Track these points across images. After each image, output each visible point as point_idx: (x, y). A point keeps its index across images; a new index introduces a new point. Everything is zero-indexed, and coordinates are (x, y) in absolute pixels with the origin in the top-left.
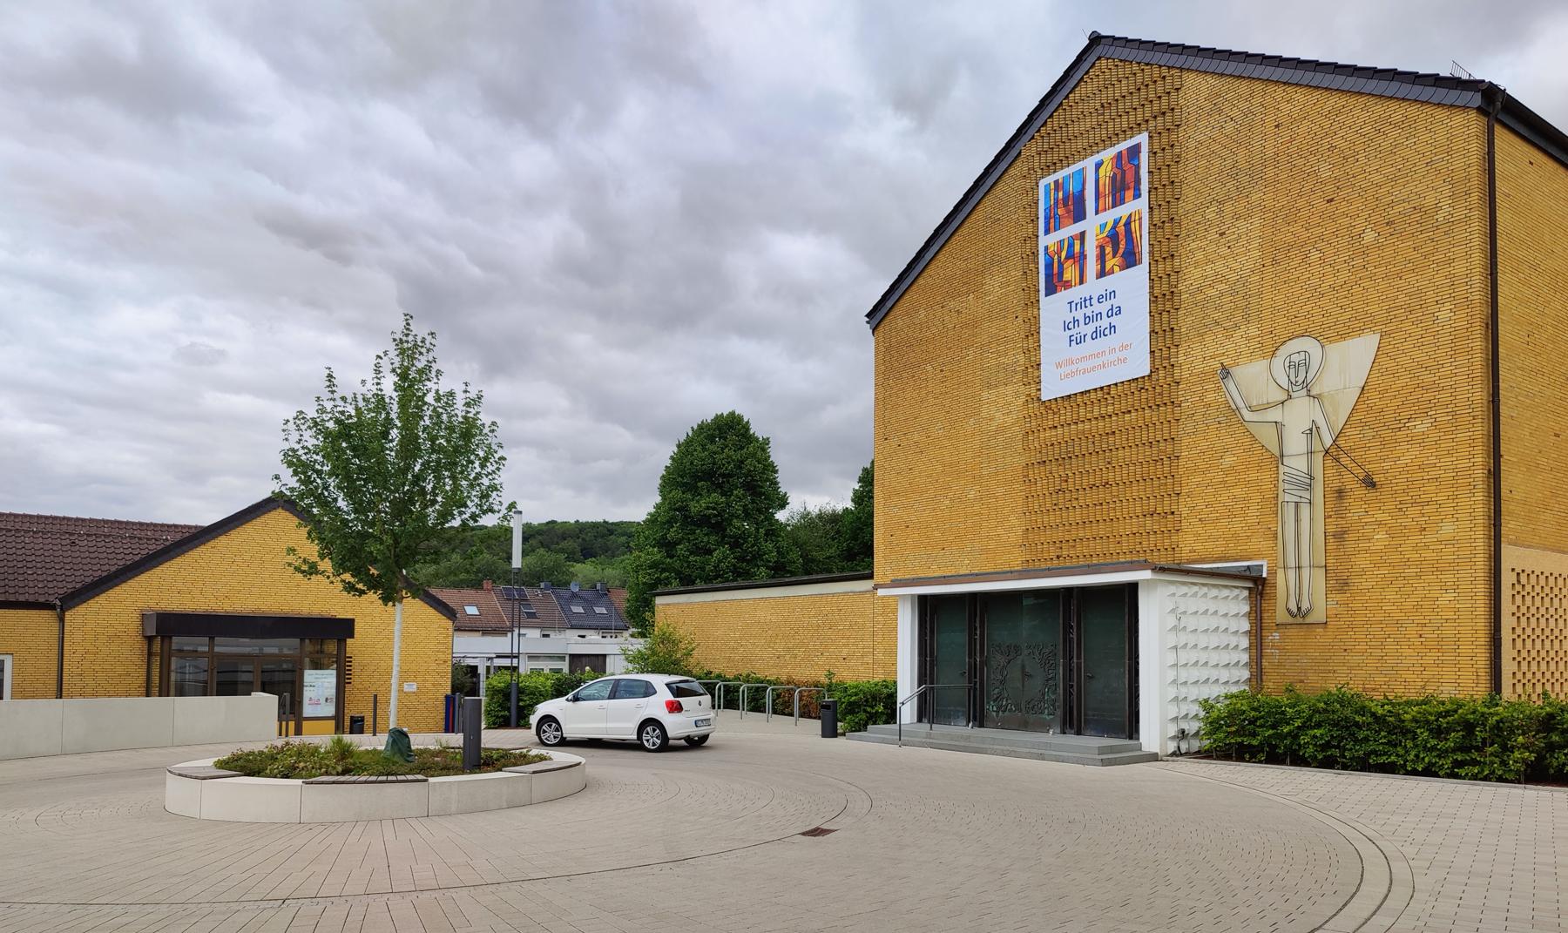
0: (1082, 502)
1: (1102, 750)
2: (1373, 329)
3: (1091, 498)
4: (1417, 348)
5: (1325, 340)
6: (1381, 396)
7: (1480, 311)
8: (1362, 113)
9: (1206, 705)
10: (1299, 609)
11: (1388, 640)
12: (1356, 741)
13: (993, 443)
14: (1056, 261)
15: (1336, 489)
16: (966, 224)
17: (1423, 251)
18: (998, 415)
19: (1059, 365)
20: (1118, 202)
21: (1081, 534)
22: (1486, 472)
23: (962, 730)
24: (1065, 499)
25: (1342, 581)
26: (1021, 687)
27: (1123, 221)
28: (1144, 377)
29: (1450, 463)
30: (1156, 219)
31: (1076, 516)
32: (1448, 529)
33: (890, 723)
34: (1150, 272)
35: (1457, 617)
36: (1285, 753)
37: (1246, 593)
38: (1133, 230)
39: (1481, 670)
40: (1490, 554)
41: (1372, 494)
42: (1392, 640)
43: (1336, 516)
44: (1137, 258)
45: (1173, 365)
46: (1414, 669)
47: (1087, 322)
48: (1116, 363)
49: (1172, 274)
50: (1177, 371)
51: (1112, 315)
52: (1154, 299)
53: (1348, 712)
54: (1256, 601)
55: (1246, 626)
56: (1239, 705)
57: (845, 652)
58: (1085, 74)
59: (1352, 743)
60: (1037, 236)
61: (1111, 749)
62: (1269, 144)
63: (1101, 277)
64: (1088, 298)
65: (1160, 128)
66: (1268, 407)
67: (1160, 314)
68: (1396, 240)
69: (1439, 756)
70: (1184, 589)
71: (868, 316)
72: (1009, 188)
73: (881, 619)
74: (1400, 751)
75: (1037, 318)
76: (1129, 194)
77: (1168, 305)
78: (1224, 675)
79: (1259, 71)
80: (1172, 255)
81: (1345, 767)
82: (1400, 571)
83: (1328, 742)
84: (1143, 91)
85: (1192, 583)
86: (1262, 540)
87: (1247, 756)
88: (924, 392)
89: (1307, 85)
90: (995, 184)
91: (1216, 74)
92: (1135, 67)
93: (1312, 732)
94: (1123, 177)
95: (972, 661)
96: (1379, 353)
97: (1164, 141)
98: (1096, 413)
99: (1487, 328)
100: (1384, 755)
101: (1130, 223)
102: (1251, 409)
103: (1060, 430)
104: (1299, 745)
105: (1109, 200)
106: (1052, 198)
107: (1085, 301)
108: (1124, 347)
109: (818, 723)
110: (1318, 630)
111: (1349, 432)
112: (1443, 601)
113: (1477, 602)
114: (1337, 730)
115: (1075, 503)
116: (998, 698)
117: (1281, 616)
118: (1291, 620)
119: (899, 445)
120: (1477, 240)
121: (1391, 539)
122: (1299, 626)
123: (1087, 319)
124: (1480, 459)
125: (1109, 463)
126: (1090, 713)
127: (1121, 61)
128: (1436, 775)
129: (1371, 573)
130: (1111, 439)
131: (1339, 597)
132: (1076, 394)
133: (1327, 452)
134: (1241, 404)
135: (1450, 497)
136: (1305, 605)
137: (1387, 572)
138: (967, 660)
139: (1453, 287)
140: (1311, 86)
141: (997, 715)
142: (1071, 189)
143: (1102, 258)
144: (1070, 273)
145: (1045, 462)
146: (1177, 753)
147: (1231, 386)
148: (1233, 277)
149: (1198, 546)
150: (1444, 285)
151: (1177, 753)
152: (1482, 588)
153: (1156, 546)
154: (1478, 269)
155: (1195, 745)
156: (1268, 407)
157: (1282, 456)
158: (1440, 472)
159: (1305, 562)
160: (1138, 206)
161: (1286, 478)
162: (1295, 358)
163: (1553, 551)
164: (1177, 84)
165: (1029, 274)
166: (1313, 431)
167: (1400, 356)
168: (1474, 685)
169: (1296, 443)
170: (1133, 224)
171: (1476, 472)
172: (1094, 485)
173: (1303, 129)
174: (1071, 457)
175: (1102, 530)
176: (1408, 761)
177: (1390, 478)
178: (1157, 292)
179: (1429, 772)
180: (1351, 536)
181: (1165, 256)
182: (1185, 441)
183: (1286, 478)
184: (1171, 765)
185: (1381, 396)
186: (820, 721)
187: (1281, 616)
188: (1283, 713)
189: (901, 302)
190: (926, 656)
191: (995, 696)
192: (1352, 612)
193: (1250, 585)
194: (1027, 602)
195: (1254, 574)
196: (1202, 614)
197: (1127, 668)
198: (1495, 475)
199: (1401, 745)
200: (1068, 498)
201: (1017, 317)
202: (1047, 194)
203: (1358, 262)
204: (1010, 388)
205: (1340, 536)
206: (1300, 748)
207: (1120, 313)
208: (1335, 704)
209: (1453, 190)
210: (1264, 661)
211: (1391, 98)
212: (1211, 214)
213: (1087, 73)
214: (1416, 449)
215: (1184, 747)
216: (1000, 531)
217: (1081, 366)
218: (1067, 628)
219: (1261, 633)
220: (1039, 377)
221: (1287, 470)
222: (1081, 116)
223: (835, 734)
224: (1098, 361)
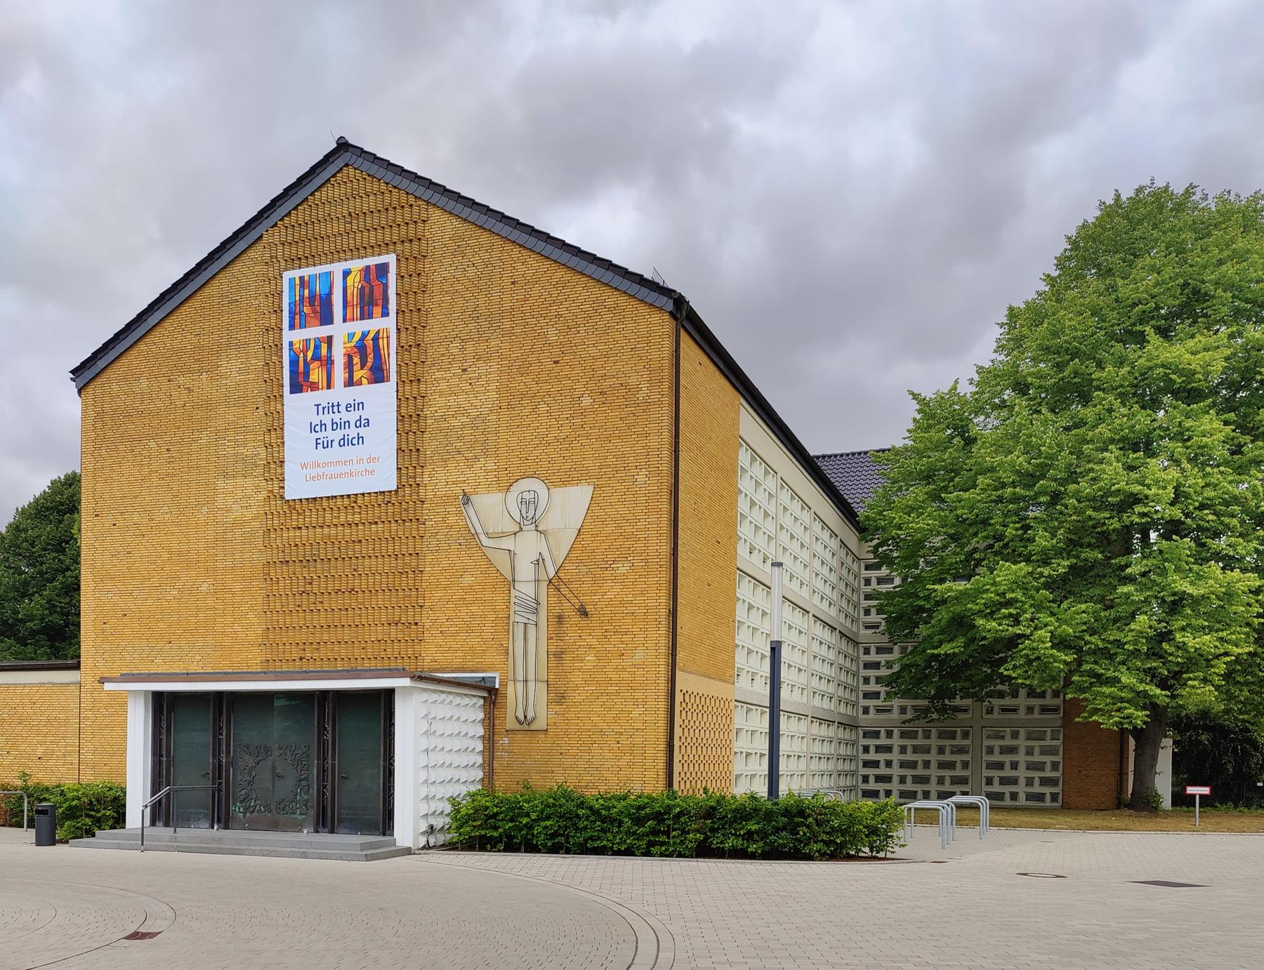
0: (326, 606)
1: (364, 847)
2: (588, 481)
3: (336, 602)
4: (621, 503)
5: (550, 484)
6: (593, 539)
7: (667, 481)
8: (583, 292)
9: (453, 800)
10: (525, 717)
11: (594, 745)
12: (577, 829)
13: (229, 535)
14: (301, 359)
15: (557, 614)
16: (199, 297)
17: (627, 422)
18: (235, 507)
19: (304, 466)
20: (366, 315)
21: (325, 637)
22: (667, 611)
23: (203, 832)
24: (308, 601)
25: (560, 695)
26: (272, 788)
27: (371, 336)
28: (390, 492)
29: (643, 602)
30: (403, 342)
31: (322, 619)
32: (639, 656)
33: (116, 828)
34: (397, 391)
35: (644, 727)
36: (520, 843)
37: (481, 702)
38: (381, 346)
39: (661, 770)
40: (668, 678)
41: (584, 622)
42: (597, 745)
43: (556, 638)
44: (385, 375)
45: (418, 484)
46: (612, 769)
47: (335, 428)
48: (364, 473)
49: (418, 397)
50: (422, 491)
51: (360, 426)
52: (401, 418)
53: (571, 805)
54: (490, 709)
55: (481, 732)
56: (484, 802)
57: (40, 751)
58: (332, 177)
59: (574, 831)
60: (281, 330)
61: (371, 846)
62: (506, 297)
63: (349, 386)
64: (335, 404)
65: (407, 254)
66: (502, 535)
67: (407, 433)
68: (607, 408)
69: (638, 839)
70: (435, 697)
71: (73, 372)
72: (249, 268)
73: (89, 714)
74: (610, 836)
75: (280, 414)
76: (377, 310)
77: (414, 428)
78: (464, 775)
79: (498, 227)
80: (419, 380)
81: (568, 852)
82: (605, 688)
83: (556, 831)
84: (391, 212)
85: (441, 692)
87: (489, 846)
88: (146, 471)
89: (539, 253)
90: (232, 261)
91: (460, 217)
92: (383, 186)
93: (543, 824)
94: (371, 292)
95: (216, 761)
96: (592, 502)
97: (411, 267)
98: (342, 519)
99: (671, 494)
100: (598, 840)
101: (378, 339)
102: (487, 534)
103: (304, 532)
104: (533, 835)
105: (357, 311)
106: (297, 293)
107: (333, 406)
108: (371, 460)
109: (32, 832)
110: (540, 736)
111: (567, 566)
112: (635, 714)
113: (659, 716)
114: (563, 821)
115: (319, 606)
116: (245, 799)
117: (511, 723)
118: (518, 727)
119: (114, 525)
120: (667, 422)
122: (524, 732)
123: (335, 425)
124: (664, 600)
125: (355, 570)
126: (343, 812)
127: (369, 175)
128: (633, 854)
130: (357, 547)
131: (557, 708)
132: (322, 498)
133: (550, 582)
134: (480, 531)
135: (642, 630)
136: (530, 715)
137: (594, 688)
138: (211, 760)
139: (648, 457)
140: (542, 255)
141: (245, 817)
142: (318, 289)
143: (349, 366)
144: (316, 375)
145: (288, 561)
146: (427, 847)
147: (471, 511)
148: (474, 413)
149: (438, 657)
150: (642, 454)
151: (427, 847)
152: (663, 705)
153: (400, 654)
154: (667, 446)
155: (441, 839)
156: (502, 535)
157: (514, 581)
158: (635, 608)
159: (531, 676)
160: (386, 324)
161: (517, 601)
162: (527, 496)
163: (704, 676)
164: (424, 215)
165: (271, 365)
166: (539, 563)
167: (608, 507)
168: (655, 782)
169: (525, 571)
170: (381, 341)
171: (661, 610)
172: (340, 590)
173: (535, 291)
174: (316, 560)
175: (347, 635)
176: (614, 844)
177: (598, 609)
178: (403, 411)
179: (629, 852)
180: (567, 657)
181: (411, 381)
182: (429, 557)
183: (517, 601)
184: (425, 858)
185: (593, 539)
186: (34, 830)
187: (511, 723)
188: (521, 808)
189: (117, 364)
190: (162, 756)
191: (242, 798)
192: (568, 721)
193: (485, 694)
194: (277, 703)
195: (488, 685)
196: (448, 720)
197: (382, 769)
198: (673, 614)
199: (609, 832)
200: (312, 600)
201: (257, 408)
202: (292, 287)
203: (577, 421)
204: (249, 482)
206: (533, 837)
207: (368, 425)
208: (562, 799)
209: (650, 376)
210: (495, 762)
211: (606, 285)
212: (454, 348)
213: (334, 176)
214: (618, 587)
215: (432, 841)
216: (237, 628)
217: (328, 470)
218: (322, 730)
219: (493, 737)
220: (282, 474)
221: (517, 594)
222: (328, 219)
223: (53, 842)
224: (344, 469)
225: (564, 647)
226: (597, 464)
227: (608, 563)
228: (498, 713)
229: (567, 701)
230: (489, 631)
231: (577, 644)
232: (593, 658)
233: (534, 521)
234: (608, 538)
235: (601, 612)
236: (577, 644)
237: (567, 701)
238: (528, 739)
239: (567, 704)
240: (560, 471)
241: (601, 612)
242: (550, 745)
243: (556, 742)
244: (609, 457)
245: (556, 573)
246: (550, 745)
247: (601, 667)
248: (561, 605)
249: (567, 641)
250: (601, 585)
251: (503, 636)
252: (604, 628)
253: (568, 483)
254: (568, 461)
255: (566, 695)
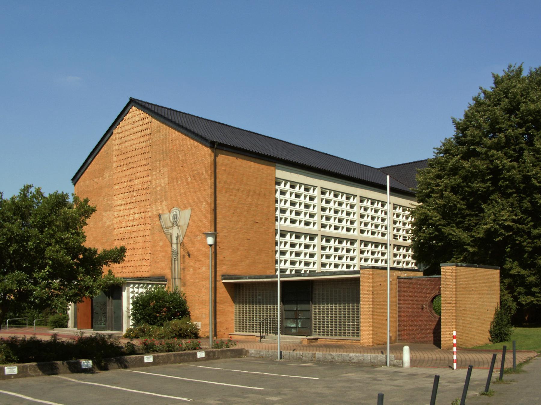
10: (521, 364)
18: (107, 221)
71: (72, 180)
180: (186, 270)
205: (184, 269)
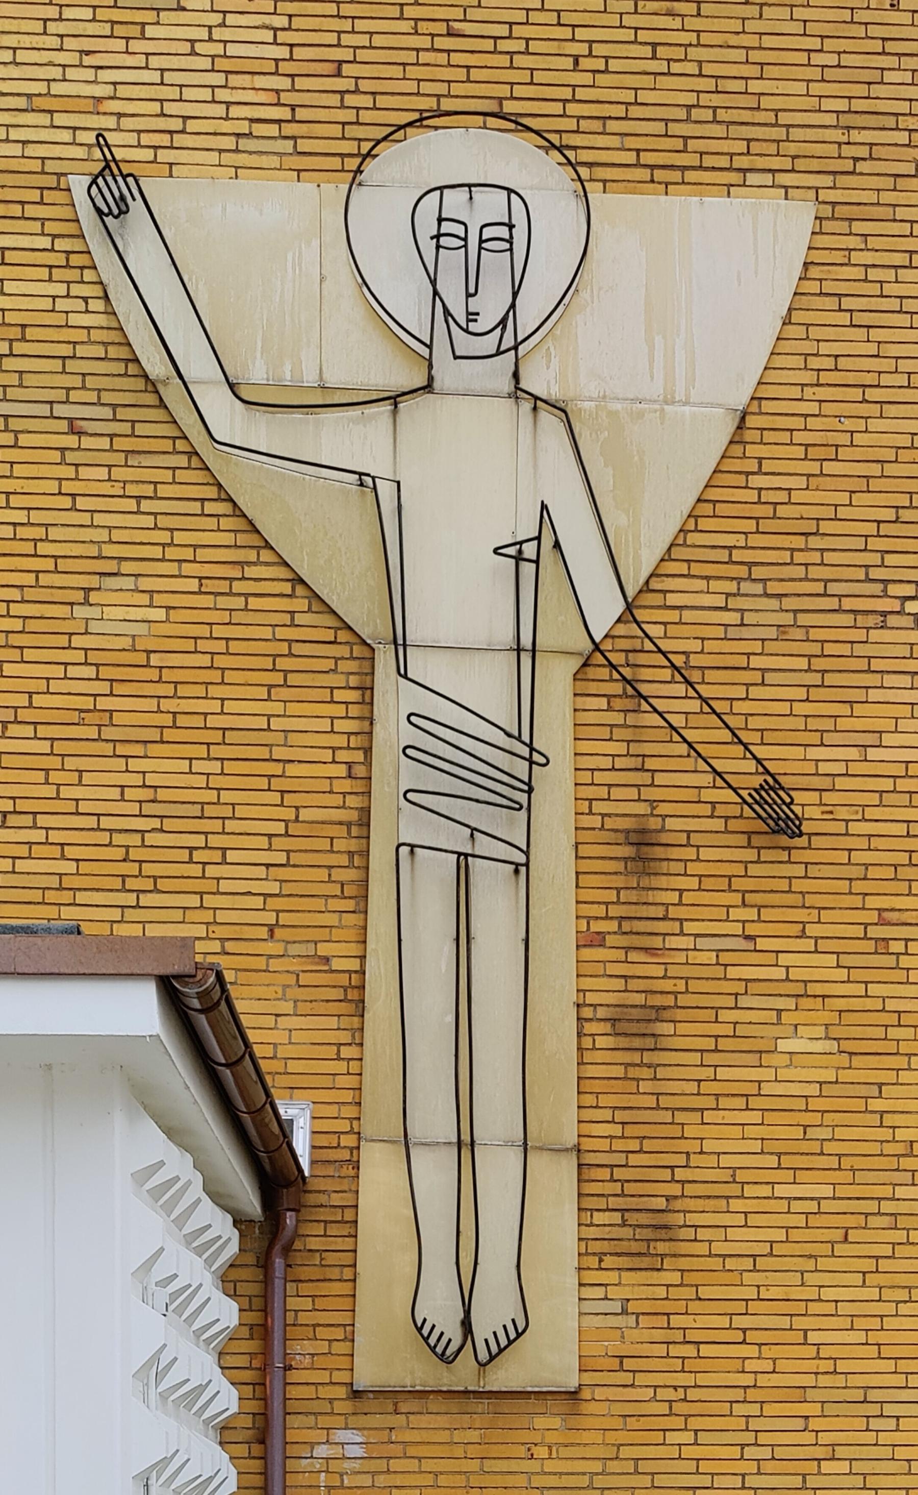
10: (467, 1326)
11: (826, 1467)
25: (644, 1218)
42: (844, 1467)
86: (288, 1007)
110: (540, 1422)
121: (844, 1059)
122: (453, 1405)
129: (766, 1191)
137: (827, 1191)
157: (400, 643)
177: (842, 813)
185: (814, 468)
192: (690, 1350)
225: (667, 985)
226: (827, 104)
227: (893, 590)
228: (307, 1303)
229: (685, 1248)
230: (255, 887)
231: (732, 972)
232: (819, 1046)
233: (508, 342)
234: (890, 469)
235: (854, 828)
236: (732, 972)
237: (685, 1248)
238: (474, 1436)
239: (684, 1263)
240: (635, 111)
241: (854, 828)
242: (597, 1467)
243: (625, 1452)
244: (889, 77)
245: (629, 607)
246: (597, 1467)
247: (863, 1091)
248: (646, 778)
249: (681, 957)
250: (859, 695)
251: (332, 920)
252: (871, 902)
253: (676, 176)
254: (676, 68)
255: (679, 1219)
